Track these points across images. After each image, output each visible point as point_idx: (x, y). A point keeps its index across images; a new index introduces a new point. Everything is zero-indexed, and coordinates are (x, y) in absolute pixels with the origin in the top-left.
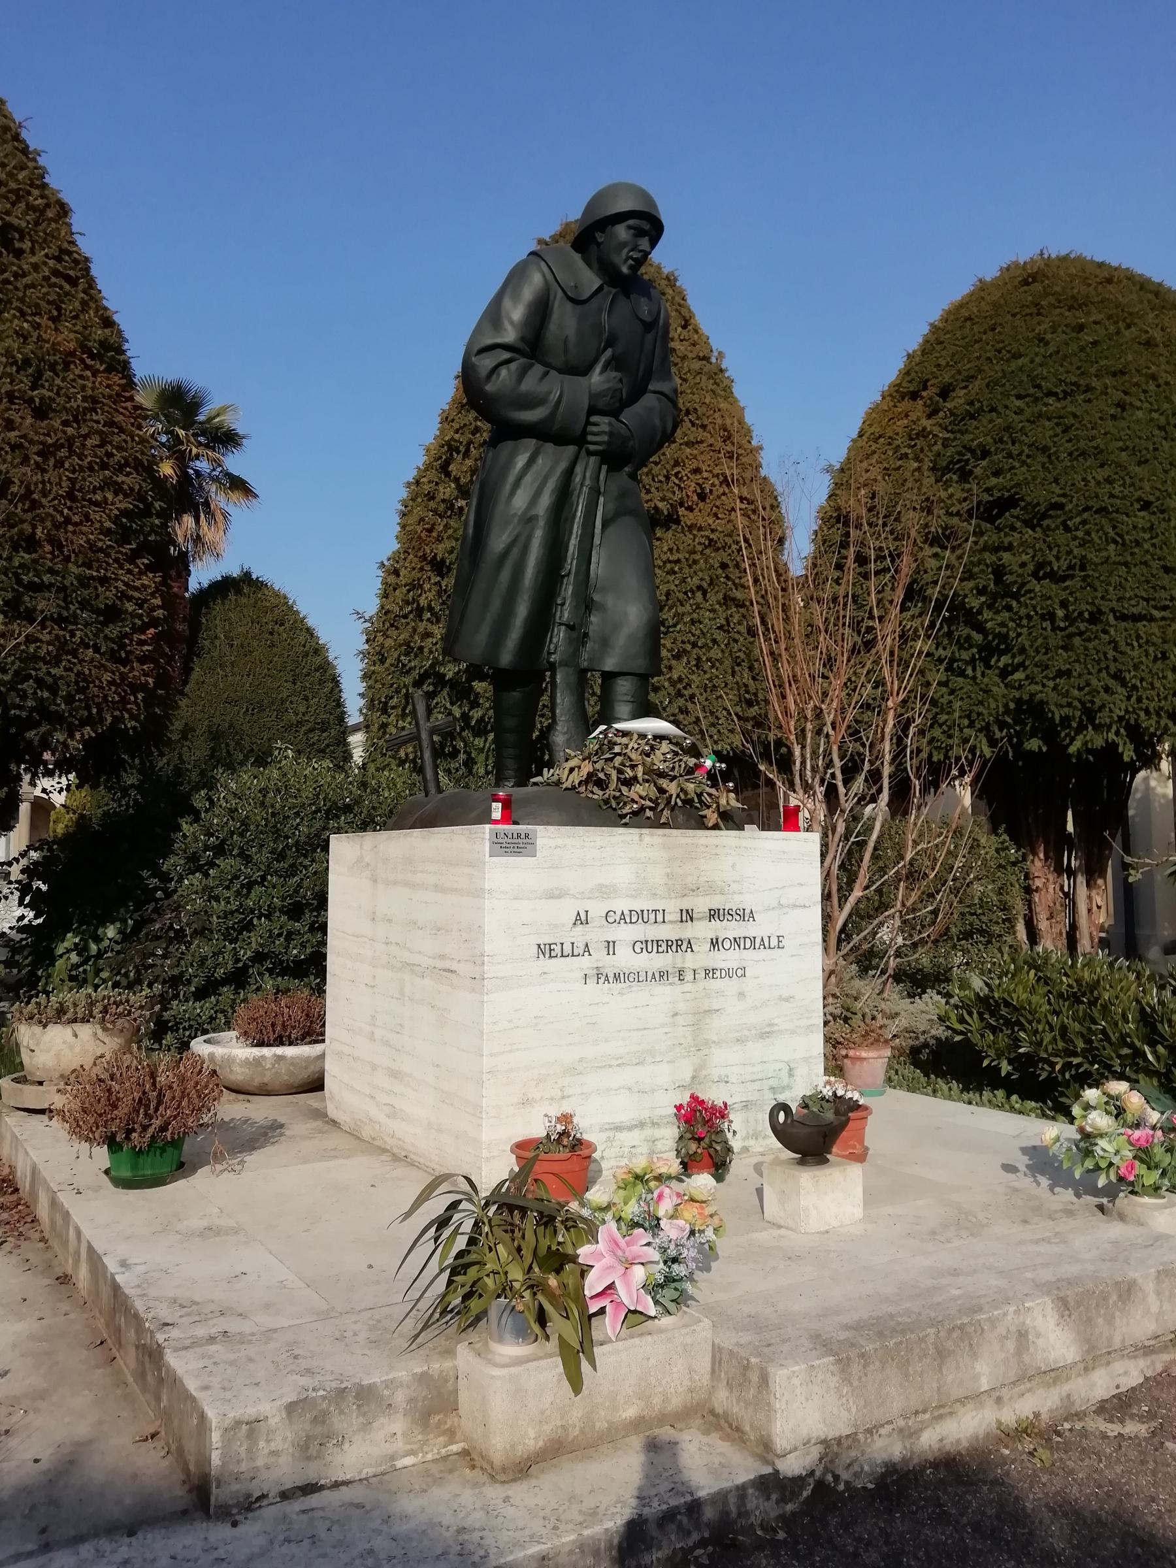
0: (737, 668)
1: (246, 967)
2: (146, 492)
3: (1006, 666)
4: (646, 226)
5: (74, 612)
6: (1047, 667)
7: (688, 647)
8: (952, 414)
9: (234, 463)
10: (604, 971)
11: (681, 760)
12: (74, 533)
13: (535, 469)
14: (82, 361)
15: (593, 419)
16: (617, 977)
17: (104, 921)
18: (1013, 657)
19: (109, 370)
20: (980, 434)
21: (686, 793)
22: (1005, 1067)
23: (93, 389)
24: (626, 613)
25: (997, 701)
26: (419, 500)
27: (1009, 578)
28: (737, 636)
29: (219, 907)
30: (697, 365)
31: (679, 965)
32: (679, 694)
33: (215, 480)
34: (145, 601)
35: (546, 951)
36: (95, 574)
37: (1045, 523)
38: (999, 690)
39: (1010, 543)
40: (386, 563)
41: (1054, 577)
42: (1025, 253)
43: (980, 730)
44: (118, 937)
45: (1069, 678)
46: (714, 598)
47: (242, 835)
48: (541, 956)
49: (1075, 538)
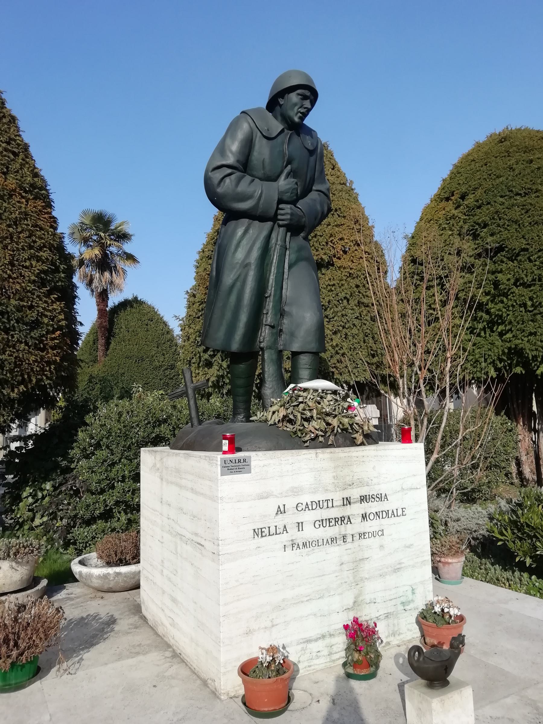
0: (366, 338)
1: (111, 509)
2: (56, 260)
3: (502, 331)
4: (307, 93)
5: (13, 325)
6: (524, 331)
7: (341, 328)
8: (467, 207)
9: (128, 247)
10: (296, 542)
11: (339, 404)
12: (14, 283)
13: (248, 236)
14: (20, 194)
15: (281, 206)
16: (304, 545)
17: (46, 479)
18: (506, 326)
19: (35, 198)
20: (483, 215)
21: (343, 425)
22: (528, 561)
23: (25, 208)
24: (303, 318)
25: (498, 348)
26: (204, 260)
27: (502, 287)
28: (365, 322)
29: (96, 478)
30: (340, 187)
31: (343, 533)
32: (337, 353)
33: (118, 255)
34: (55, 316)
35: (259, 533)
36: (25, 304)
37: (519, 258)
38: (499, 343)
39: (501, 269)
40: (189, 291)
41: (526, 285)
42: (498, 128)
43: (490, 364)
44: (52, 489)
45: (535, 336)
46: (353, 303)
47: (108, 438)
48: (256, 536)
49: (535, 265)
